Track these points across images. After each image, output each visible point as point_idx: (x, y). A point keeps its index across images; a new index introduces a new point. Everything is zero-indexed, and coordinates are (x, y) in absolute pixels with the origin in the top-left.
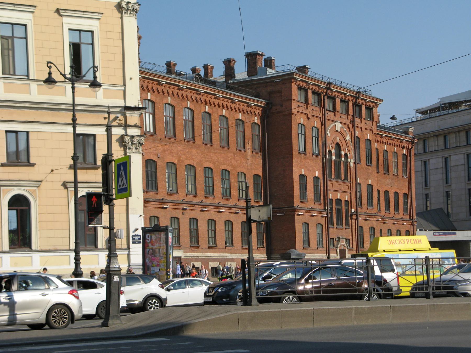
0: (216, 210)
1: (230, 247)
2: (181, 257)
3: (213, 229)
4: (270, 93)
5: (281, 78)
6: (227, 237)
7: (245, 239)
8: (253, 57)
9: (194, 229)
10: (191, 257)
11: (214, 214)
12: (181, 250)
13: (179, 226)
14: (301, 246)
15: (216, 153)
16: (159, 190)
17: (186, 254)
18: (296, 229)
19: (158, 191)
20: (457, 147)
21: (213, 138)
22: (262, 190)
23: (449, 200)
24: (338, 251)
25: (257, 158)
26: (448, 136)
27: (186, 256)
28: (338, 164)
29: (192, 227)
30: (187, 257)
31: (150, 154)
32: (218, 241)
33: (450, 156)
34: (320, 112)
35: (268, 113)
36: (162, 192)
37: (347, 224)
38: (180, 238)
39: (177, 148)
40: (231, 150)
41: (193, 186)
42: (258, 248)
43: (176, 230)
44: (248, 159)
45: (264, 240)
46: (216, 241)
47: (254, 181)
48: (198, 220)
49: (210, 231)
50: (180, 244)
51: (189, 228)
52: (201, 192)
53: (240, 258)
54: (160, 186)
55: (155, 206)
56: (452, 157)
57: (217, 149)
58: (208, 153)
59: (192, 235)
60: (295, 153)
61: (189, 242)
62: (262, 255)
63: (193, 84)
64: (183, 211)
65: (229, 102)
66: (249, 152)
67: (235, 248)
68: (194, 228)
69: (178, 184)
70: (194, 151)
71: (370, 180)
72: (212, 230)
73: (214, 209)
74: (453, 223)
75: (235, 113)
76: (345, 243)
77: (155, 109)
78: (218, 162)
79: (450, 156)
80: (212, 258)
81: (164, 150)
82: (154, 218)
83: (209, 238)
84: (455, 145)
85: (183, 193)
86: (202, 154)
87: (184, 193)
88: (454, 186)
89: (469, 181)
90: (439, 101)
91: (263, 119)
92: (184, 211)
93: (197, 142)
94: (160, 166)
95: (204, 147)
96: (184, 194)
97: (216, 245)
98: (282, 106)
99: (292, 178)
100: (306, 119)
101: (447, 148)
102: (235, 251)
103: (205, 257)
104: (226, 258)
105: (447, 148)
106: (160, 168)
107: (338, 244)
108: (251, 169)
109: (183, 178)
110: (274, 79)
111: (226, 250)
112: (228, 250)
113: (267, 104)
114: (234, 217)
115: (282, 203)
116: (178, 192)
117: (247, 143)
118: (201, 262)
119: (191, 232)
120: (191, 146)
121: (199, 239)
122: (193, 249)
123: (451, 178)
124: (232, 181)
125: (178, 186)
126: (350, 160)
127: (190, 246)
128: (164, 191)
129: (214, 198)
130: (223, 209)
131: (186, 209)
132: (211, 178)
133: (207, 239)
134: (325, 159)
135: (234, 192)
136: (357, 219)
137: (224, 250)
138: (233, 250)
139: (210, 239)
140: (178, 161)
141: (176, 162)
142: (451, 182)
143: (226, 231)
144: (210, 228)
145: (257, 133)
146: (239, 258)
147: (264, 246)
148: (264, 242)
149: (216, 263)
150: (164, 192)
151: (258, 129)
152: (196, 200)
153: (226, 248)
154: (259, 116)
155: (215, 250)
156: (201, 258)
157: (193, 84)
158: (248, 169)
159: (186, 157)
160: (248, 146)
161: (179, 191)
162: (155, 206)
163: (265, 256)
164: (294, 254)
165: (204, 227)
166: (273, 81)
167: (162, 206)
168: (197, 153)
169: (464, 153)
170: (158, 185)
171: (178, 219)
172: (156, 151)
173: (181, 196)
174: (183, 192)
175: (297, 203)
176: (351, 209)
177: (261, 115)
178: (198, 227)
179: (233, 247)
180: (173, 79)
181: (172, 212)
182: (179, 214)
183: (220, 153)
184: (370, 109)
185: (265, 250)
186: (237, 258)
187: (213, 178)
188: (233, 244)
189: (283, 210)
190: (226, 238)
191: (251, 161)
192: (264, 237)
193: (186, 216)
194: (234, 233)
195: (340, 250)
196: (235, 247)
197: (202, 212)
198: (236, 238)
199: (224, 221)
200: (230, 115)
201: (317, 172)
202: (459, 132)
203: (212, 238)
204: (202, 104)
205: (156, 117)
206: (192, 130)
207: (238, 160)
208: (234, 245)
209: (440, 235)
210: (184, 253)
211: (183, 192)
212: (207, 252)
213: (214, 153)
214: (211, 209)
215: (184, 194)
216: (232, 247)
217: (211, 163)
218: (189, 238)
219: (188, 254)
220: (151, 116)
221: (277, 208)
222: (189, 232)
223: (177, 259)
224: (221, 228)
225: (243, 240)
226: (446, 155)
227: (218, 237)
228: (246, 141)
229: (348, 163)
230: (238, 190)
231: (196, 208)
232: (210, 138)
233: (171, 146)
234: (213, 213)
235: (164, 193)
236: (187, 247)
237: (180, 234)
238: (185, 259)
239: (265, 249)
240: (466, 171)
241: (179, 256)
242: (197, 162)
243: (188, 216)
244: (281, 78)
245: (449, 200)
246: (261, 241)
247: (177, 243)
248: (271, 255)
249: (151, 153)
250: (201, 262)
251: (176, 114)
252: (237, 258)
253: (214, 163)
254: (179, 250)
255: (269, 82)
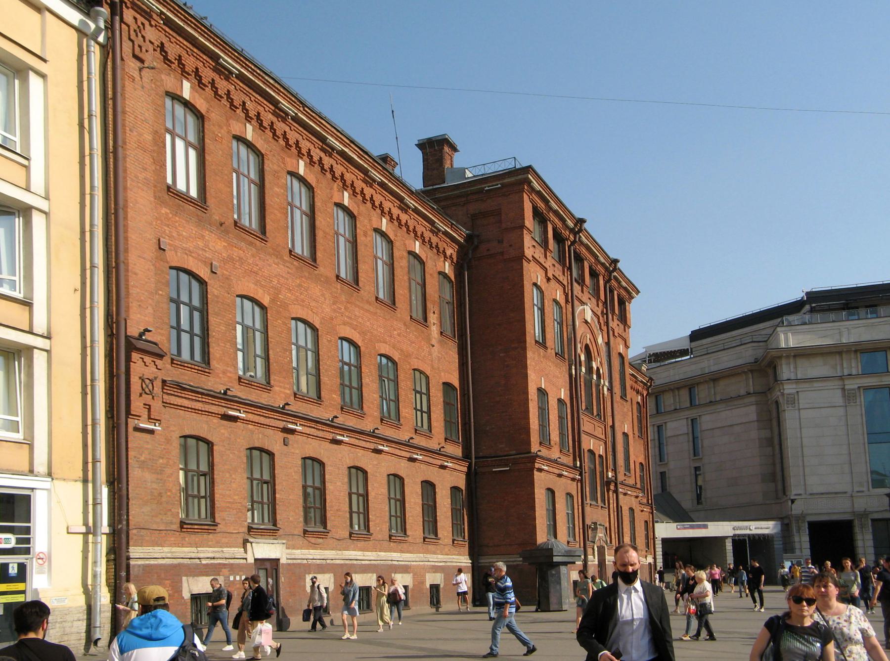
0: (368, 445)
1: (400, 538)
2: (279, 560)
3: (361, 491)
4: (474, 217)
5: (501, 182)
6: (393, 513)
7: (428, 521)
8: (436, 148)
9: (315, 488)
10: (305, 562)
11: (362, 455)
12: (280, 541)
13: (273, 476)
14: (544, 536)
15: (367, 311)
16: (214, 363)
17: (294, 551)
18: (536, 500)
19: (212, 368)
20: (676, 409)
21: (360, 274)
22: (460, 418)
23: (700, 474)
24: (596, 549)
25: (450, 349)
26: (662, 396)
27: (293, 557)
28: (588, 384)
29: (309, 483)
30: (295, 561)
31: (186, 254)
32: (374, 521)
33: (665, 423)
34: (564, 275)
35: (470, 256)
36: (224, 373)
37: (603, 501)
38: (277, 507)
39: (270, 266)
40: (399, 315)
41: (312, 379)
42: (455, 542)
43: (265, 486)
44: (433, 346)
45: (464, 524)
46: (368, 521)
47: (444, 397)
48: (324, 464)
49: (354, 497)
50: (275, 524)
51: (300, 484)
52: (332, 396)
53: (455, 564)
54: (218, 355)
55: (199, 406)
56: (669, 425)
57: (368, 302)
58: (349, 305)
59: (308, 502)
60: (530, 341)
61: (302, 519)
62: (461, 557)
63: (314, 115)
64: (286, 435)
65: (396, 204)
66: (435, 330)
67: (409, 539)
68: (314, 484)
69: (271, 361)
70: (316, 290)
71: (626, 425)
72: (359, 495)
73: (364, 442)
74: (690, 514)
75: (406, 235)
76: (603, 535)
77: (203, 137)
78: (372, 333)
79: (665, 423)
80: (359, 562)
81: (231, 259)
82: (197, 444)
83: (351, 512)
84: (673, 408)
85: (285, 388)
86: (334, 303)
87: (289, 390)
88: (672, 465)
89: (695, 456)
90: (644, 350)
91: (459, 268)
92: (290, 436)
93: (322, 270)
94: (217, 297)
95: (339, 287)
96: (288, 392)
97: (368, 531)
98: (500, 242)
99: (526, 393)
100: (545, 280)
101: (666, 413)
102: (411, 548)
103: (342, 562)
104: (390, 562)
105: (666, 413)
106: (217, 302)
107: (595, 537)
108: (439, 368)
109: (286, 350)
110: (483, 186)
111: (392, 544)
112: (395, 544)
113: (468, 238)
114: (407, 468)
115: (503, 446)
116: (272, 382)
117: (430, 311)
118: (332, 575)
119: (306, 495)
120: (307, 274)
121: (328, 515)
122: (313, 540)
123: (667, 454)
124: (402, 385)
125: (271, 367)
126: (604, 382)
127: (305, 532)
128: (230, 372)
129: (362, 416)
130: (385, 444)
131: (292, 432)
132: (357, 391)
133: (348, 515)
134: (573, 367)
135: (407, 412)
136: (616, 491)
137: (386, 544)
138: (405, 546)
139: (355, 516)
140: (273, 301)
141: (266, 301)
142: (667, 459)
143: (389, 499)
144: (354, 490)
145: (448, 297)
146: (418, 563)
147: (464, 538)
148: (464, 529)
149: (370, 575)
150: (229, 374)
151: (448, 290)
152: (324, 413)
153: (390, 538)
154: (452, 262)
155: (367, 543)
156: (332, 562)
157: (314, 115)
158: (433, 367)
159: (293, 297)
160: (433, 318)
161: (275, 380)
162: (199, 406)
163: (467, 559)
164: (559, 552)
165: (339, 484)
166: (481, 191)
167: (222, 410)
168: (323, 295)
169: (687, 418)
170: (211, 350)
171: (271, 455)
172: (205, 251)
173: (279, 396)
174: (286, 386)
175: (535, 447)
176: (607, 471)
177: (455, 260)
178: (323, 482)
179: (406, 539)
180: (261, 73)
181: (252, 432)
182: (273, 441)
183: (376, 313)
184: (622, 303)
185: (467, 546)
186: (414, 563)
187: (361, 367)
188: (404, 531)
189: (507, 459)
190: (391, 516)
191: (439, 352)
192: (464, 520)
193: (293, 450)
194: (407, 505)
195: (597, 547)
196: (410, 538)
197: (335, 446)
198: (412, 516)
199: (386, 475)
200: (396, 236)
201: (563, 390)
202: (678, 389)
203: (358, 513)
204: (336, 185)
205: (207, 157)
206: (310, 238)
207: (414, 343)
208: (408, 533)
209: (685, 528)
210: (287, 548)
211: (286, 386)
212: (347, 549)
213: (362, 308)
214: (357, 442)
215: (288, 392)
216: (403, 538)
217: (355, 330)
218: (301, 509)
219: (298, 553)
220: (192, 153)
221: (492, 457)
222: (300, 492)
223: (268, 565)
224: (378, 491)
225: (425, 522)
226: (659, 423)
227: (374, 513)
228: (429, 305)
229: (601, 387)
230: (414, 409)
231: (320, 434)
232: (354, 274)
233: (253, 256)
234: (361, 452)
235: (230, 377)
236: (296, 533)
237: (277, 496)
238: (289, 564)
239: (467, 543)
240: (691, 444)
241: (273, 556)
242: (323, 318)
243: (297, 451)
244: (501, 182)
245: (700, 474)
246: (459, 526)
247: (266, 520)
248: (481, 557)
249: (190, 251)
250: (332, 575)
251: (268, 178)
252: (414, 563)
253: (363, 333)
254: (272, 541)
255: (473, 193)
